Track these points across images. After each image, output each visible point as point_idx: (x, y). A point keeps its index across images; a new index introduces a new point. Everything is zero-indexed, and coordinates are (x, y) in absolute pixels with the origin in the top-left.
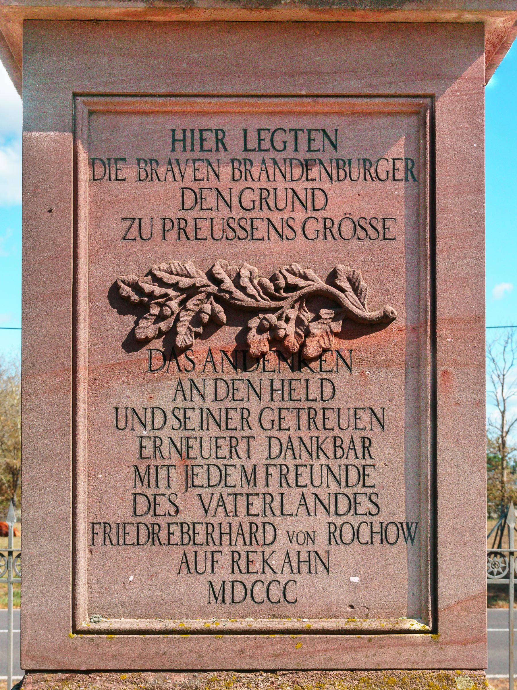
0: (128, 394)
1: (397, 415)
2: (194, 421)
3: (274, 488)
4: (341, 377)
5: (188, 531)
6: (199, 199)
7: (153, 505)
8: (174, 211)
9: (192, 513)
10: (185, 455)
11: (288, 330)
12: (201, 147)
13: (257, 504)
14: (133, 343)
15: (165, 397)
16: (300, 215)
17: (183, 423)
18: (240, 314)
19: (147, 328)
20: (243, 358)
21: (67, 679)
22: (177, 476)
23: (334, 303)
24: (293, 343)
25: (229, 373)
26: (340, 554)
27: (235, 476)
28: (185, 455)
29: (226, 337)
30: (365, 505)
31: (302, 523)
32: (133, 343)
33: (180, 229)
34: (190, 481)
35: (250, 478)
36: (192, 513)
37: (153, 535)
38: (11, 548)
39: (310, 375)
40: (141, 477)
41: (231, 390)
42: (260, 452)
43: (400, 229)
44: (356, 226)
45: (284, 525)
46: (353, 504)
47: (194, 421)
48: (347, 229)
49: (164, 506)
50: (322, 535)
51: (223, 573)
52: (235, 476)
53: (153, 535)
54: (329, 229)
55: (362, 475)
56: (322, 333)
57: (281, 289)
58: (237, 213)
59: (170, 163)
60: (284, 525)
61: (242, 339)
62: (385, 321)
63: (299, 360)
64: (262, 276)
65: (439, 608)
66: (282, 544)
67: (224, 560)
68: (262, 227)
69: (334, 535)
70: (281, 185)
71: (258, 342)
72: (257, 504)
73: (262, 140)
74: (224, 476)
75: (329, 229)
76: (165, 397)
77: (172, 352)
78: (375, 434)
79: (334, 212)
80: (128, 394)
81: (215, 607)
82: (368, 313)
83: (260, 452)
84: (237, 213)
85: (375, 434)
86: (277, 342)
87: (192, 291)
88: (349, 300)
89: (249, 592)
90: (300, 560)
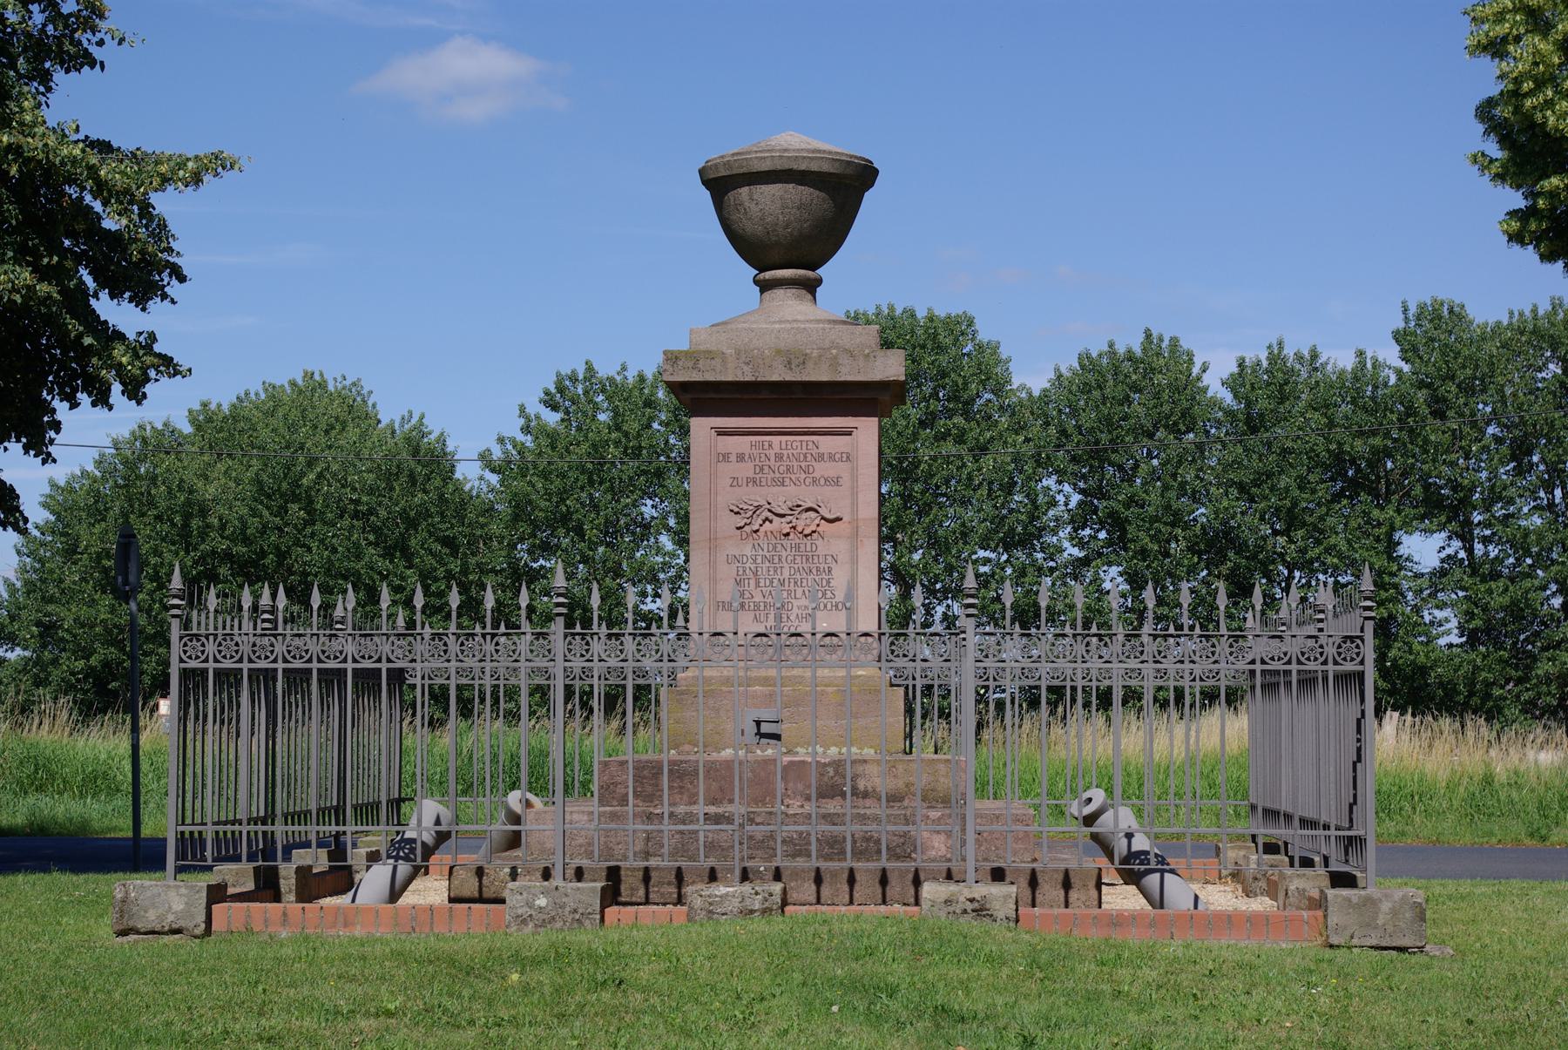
4: (819, 542)
5: (757, 606)
6: (762, 469)
7: (742, 595)
8: (751, 474)
9: (758, 598)
10: (755, 574)
17: (755, 561)
28: (755, 574)
30: (829, 594)
33: (753, 481)
34: (757, 585)
40: (738, 583)
41: (775, 548)
42: (786, 574)
49: (747, 595)
59: (1033, 882)
64: (875, 652)
65: (749, 378)
66: (795, 610)
68: (787, 481)
75: (815, 481)
78: (833, 565)
83: (786, 574)
85: (833, 565)
90: (476, 894)
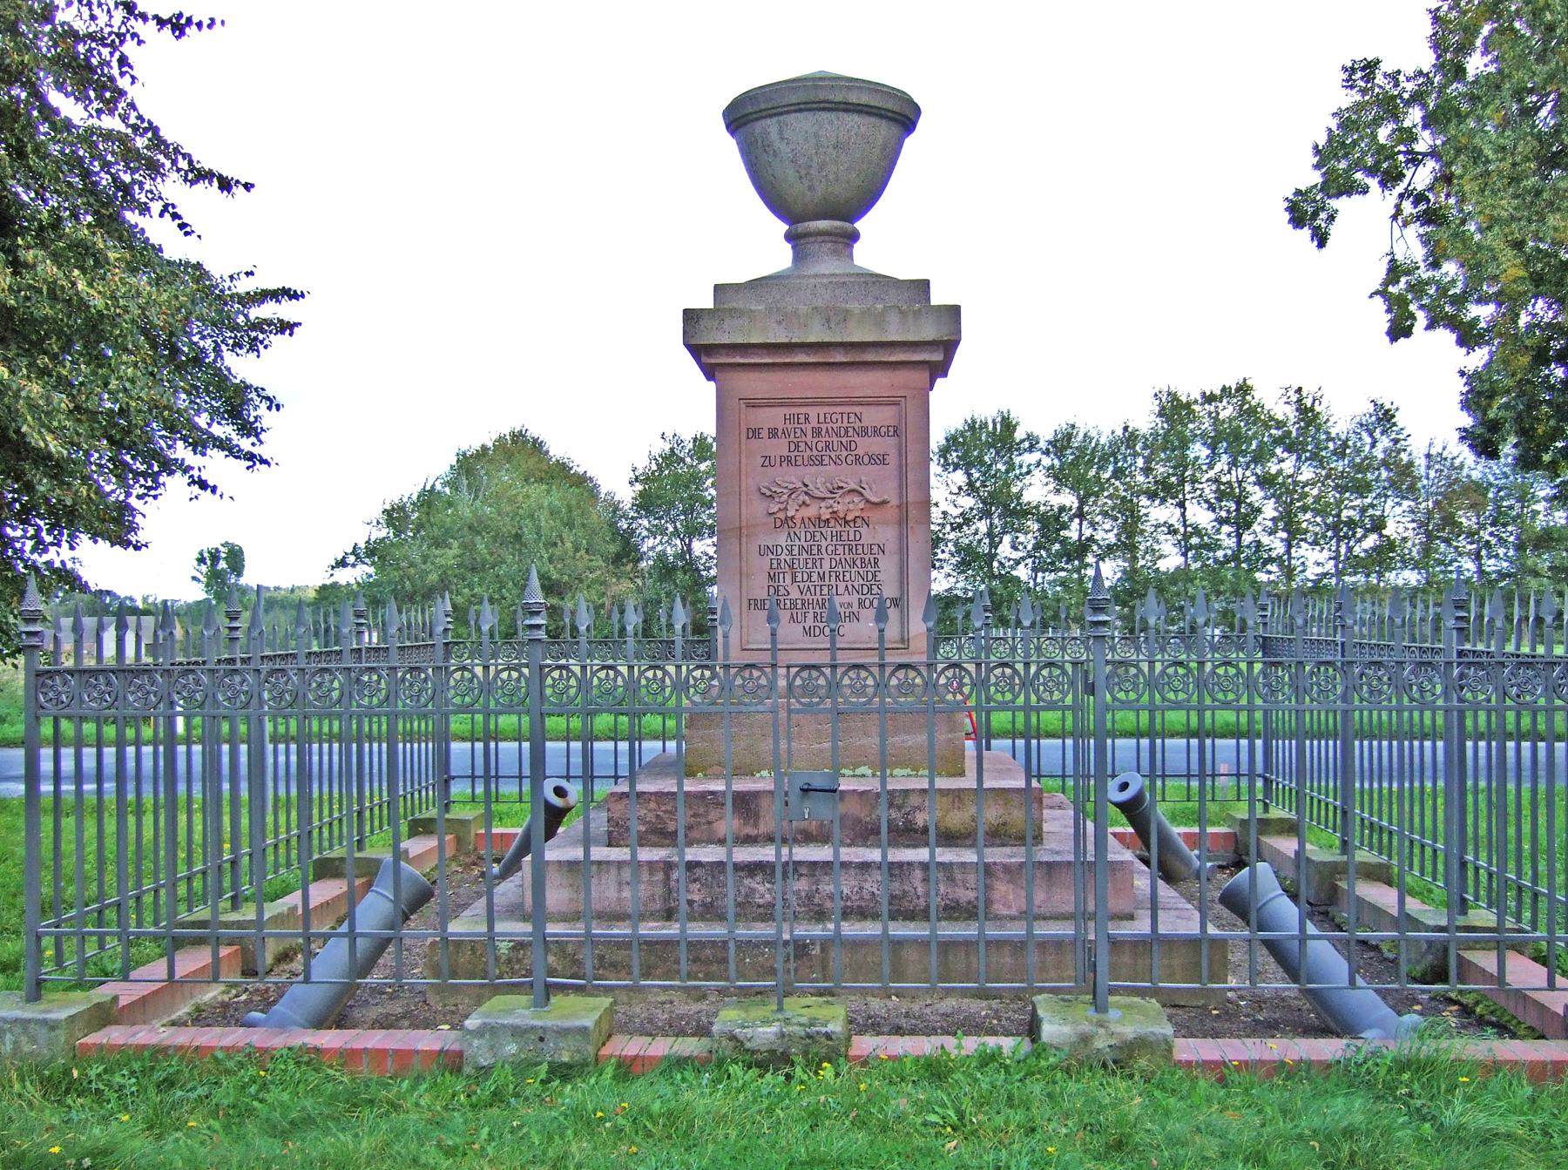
1: (891, 547)
2: (796, 552)
3: (833, 582)
4: (864, 530)
5: (794, 603)
6: (797, 447)
7: (777, 591)
8: (786, 453)
9: (795, 594)
10: (791, 567)
13: (825, 591)
16: (844, 453)
17: (791, 552)
22: (788, 577)
26: (863, 612)
27: (815, 577)
28: (791, 567)
31: (846, 599)
34: (794, 580)
35: (822, 578)
36: (795, 594)
42: (826, 566)
43: (892, 459)
44: (870, 458)
46: (870, 589)
47: (796, 552)
48: (866, 459)
49: (782, 591)
50: (856, 605)
51: (810, 622)
52: (815, 577)
54: (858, 459)
55: (874, 576)
57: (1400, 130)
58: (815, 452)
62: (884, 502)
67: (810, 616)
68: (826, 459)
69: (861, 603)
70: (835, 439)
72: (825, 591)
73: (780, 1003)
74: (810, 576)
75: (858, 459)
79: (860, 451)
81: (807, 638)
83: (826, 566)
84: (815, 452)
87: (793, 491)
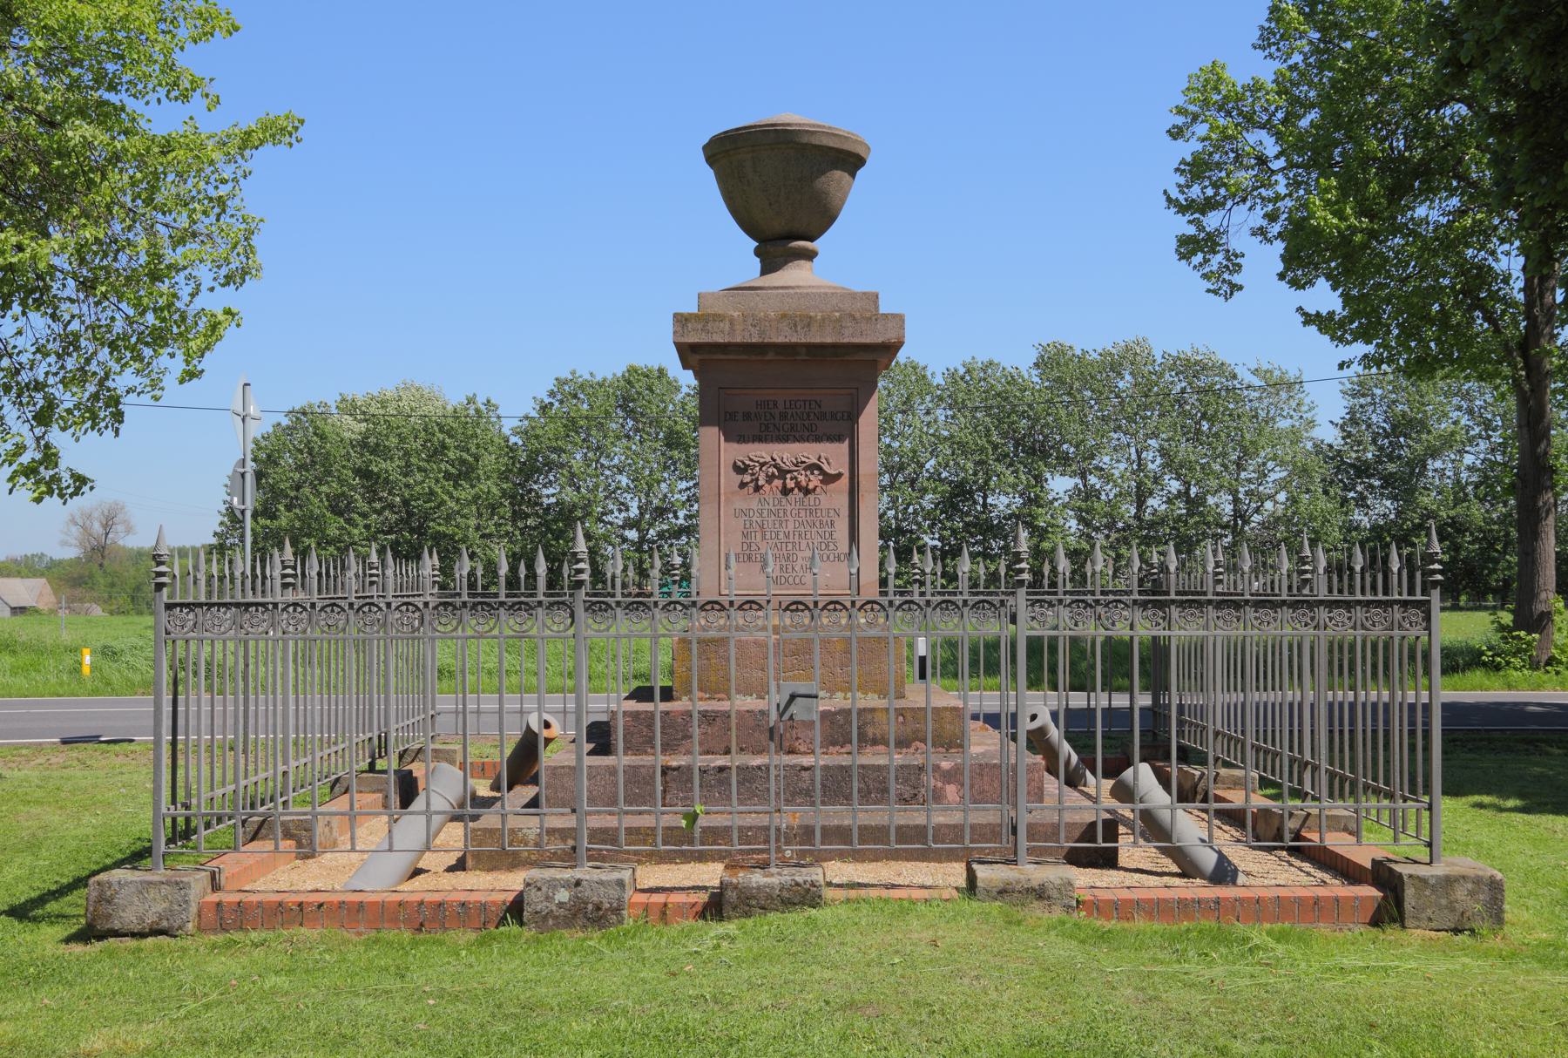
0: (740, 504)
6: (767, 427)
7: (749, 546)
11: (802, 478)
12: (664, 798)
14: (743, 485)
15: (754, 505)
18: (783, 473)
19: (747, 478)
20: (786, 491)
21: (1314, 909)
23: (820, 468)
24: (804, 484)
25: (779, 495)
27: (781, 536)
29: (778, 483)
32: (743, 485)
34: (764, 538)
35: (787, 537)
37: (749, 558)
38: (738, 692)
39: (811, 496)
42: (791, 526)
45: (800, 554)
46: (827, 546)
52: (781, 536)
53: (749, 558)
56: (815, 480)
60: (800, 554)
61: (784, 485)
62: (839, 475)
63: (807, 492)
66: (800, 561)
71: (790, 484)
76: (754, 505)
77: (757, 488)
80: (740, 504)
82: (832, 472)
83: (791, 526)
86: (798, 484)
87: (762, 465)
88: (825, 467)
89: (787, 580)
